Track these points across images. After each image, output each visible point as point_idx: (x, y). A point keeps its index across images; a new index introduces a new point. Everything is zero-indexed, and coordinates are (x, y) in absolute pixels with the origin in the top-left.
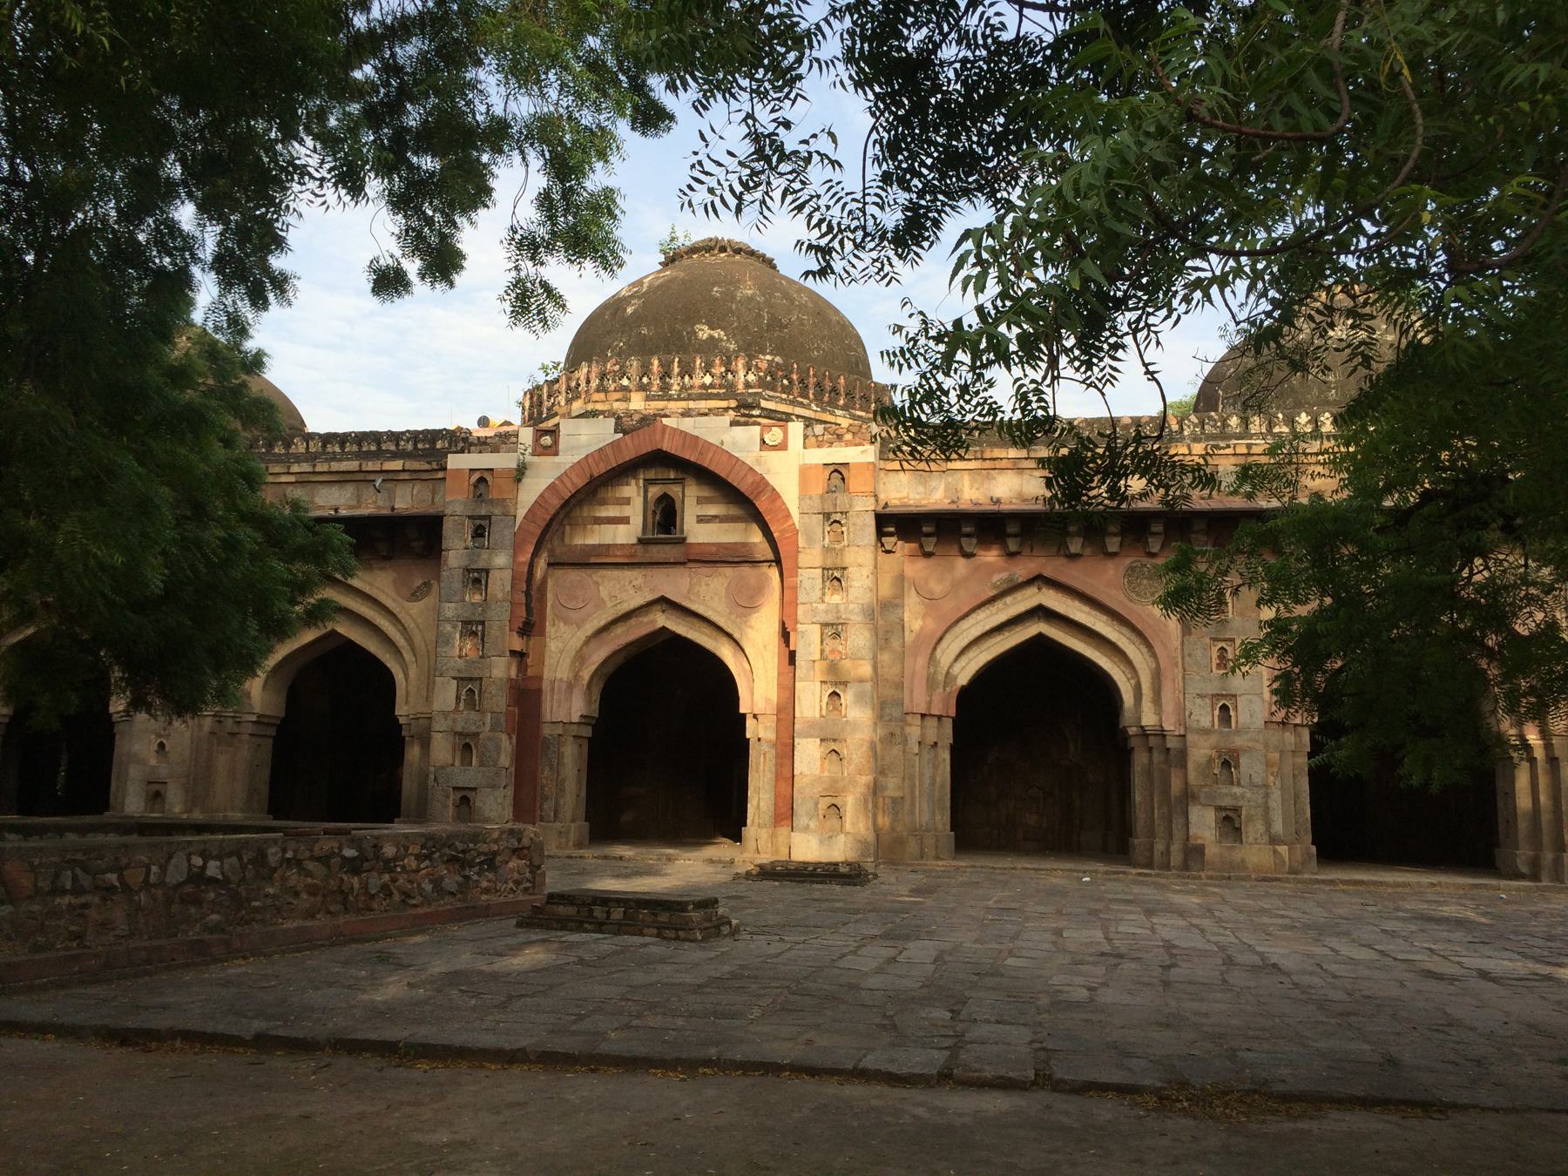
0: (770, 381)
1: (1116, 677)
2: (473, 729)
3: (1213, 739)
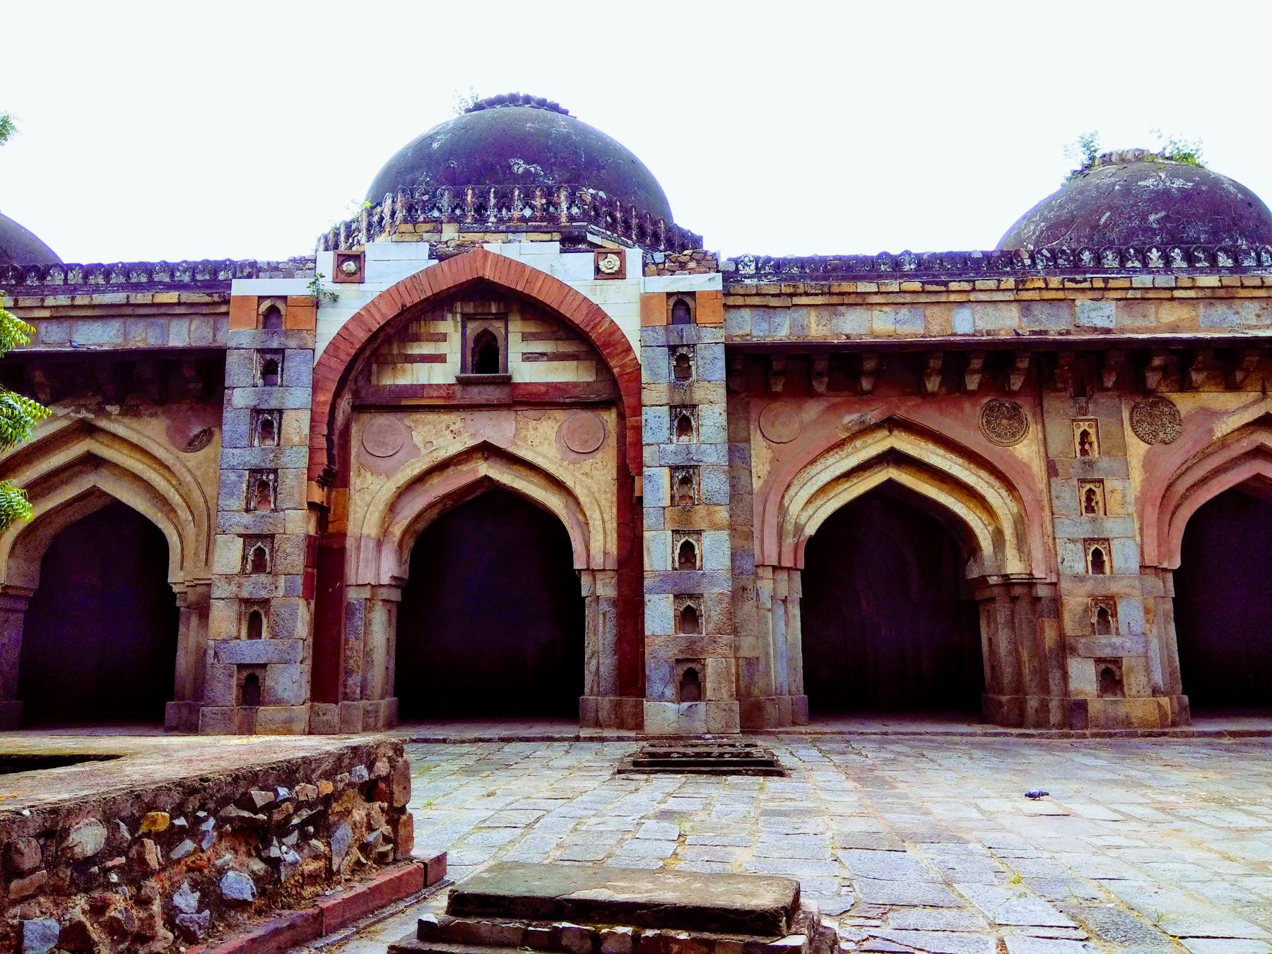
0: (595, 214)
2: (264, 594)
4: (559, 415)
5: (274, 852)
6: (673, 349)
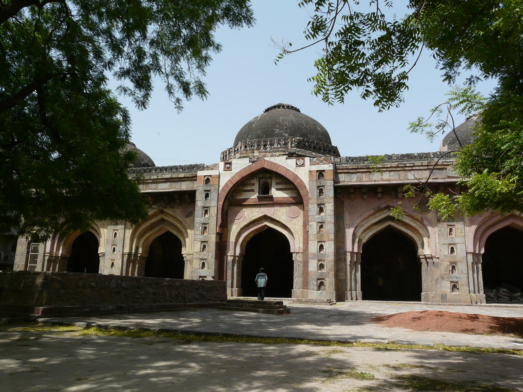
2: (205, 257)
6: (318, 187)
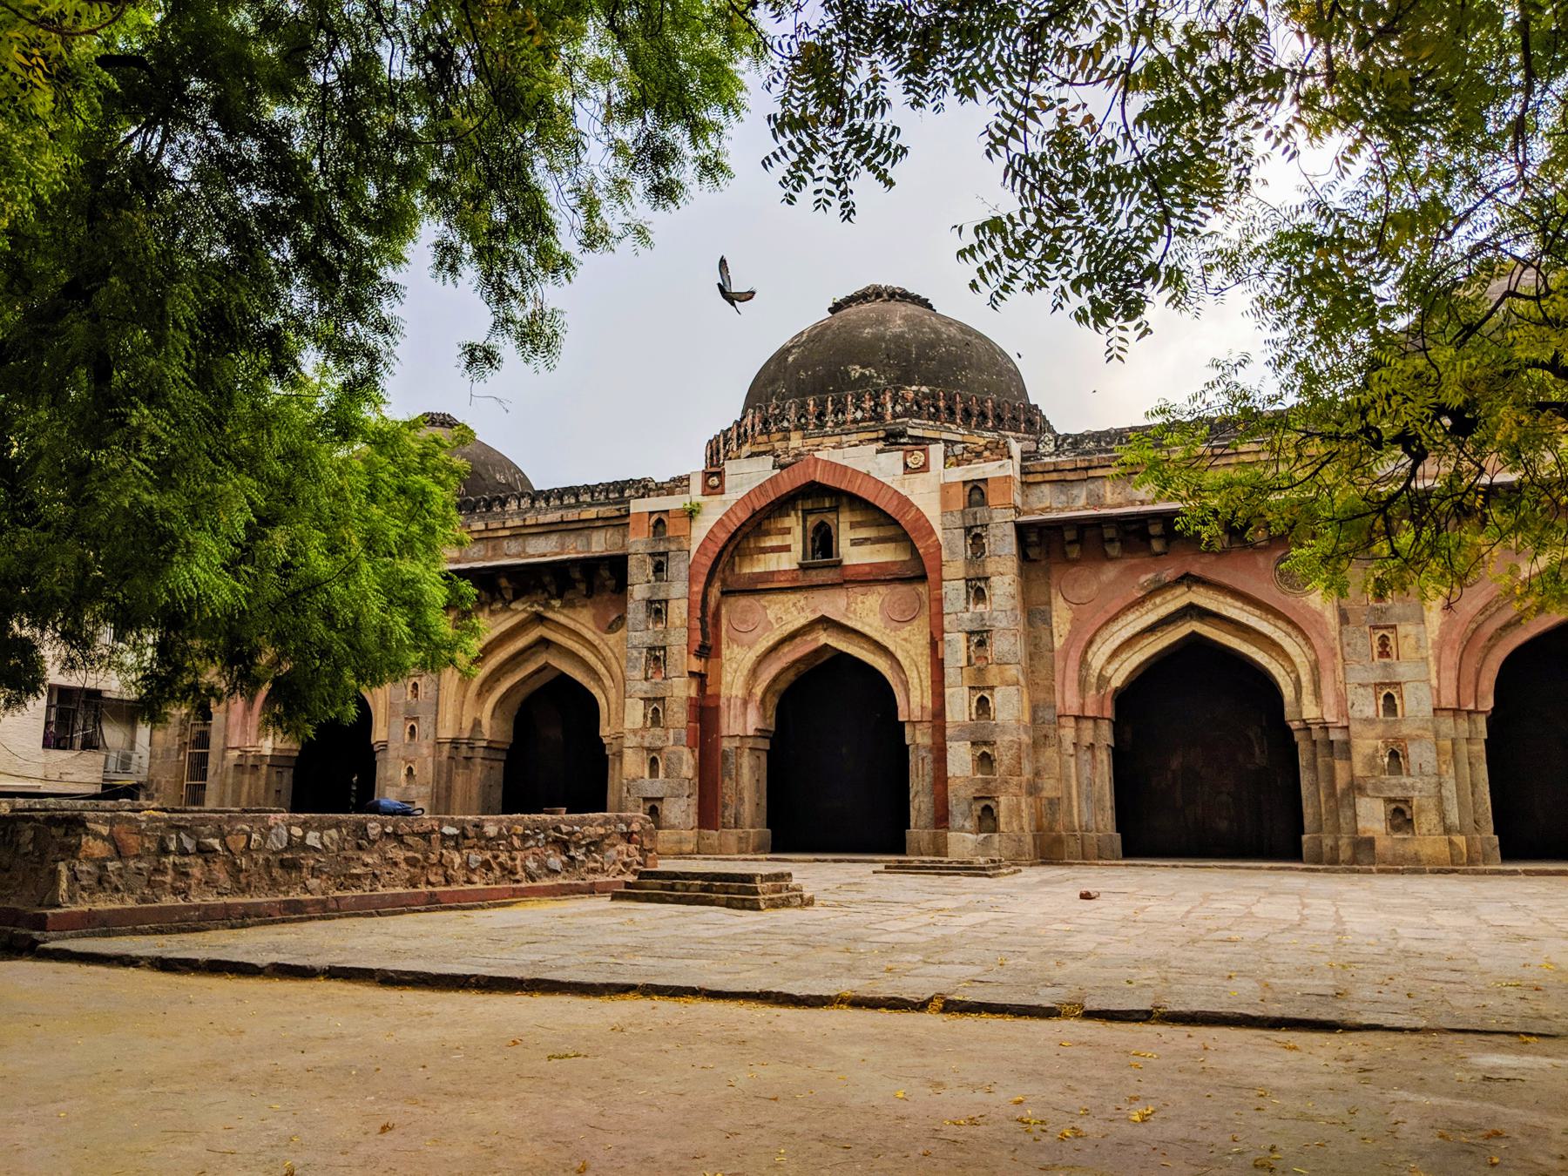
0: (917, 409)
1: (1274, 672)
2: (659, 744)
3: (1379, 729)
4: (882, 589)
5: (572, 853)
6: (968, 530)
